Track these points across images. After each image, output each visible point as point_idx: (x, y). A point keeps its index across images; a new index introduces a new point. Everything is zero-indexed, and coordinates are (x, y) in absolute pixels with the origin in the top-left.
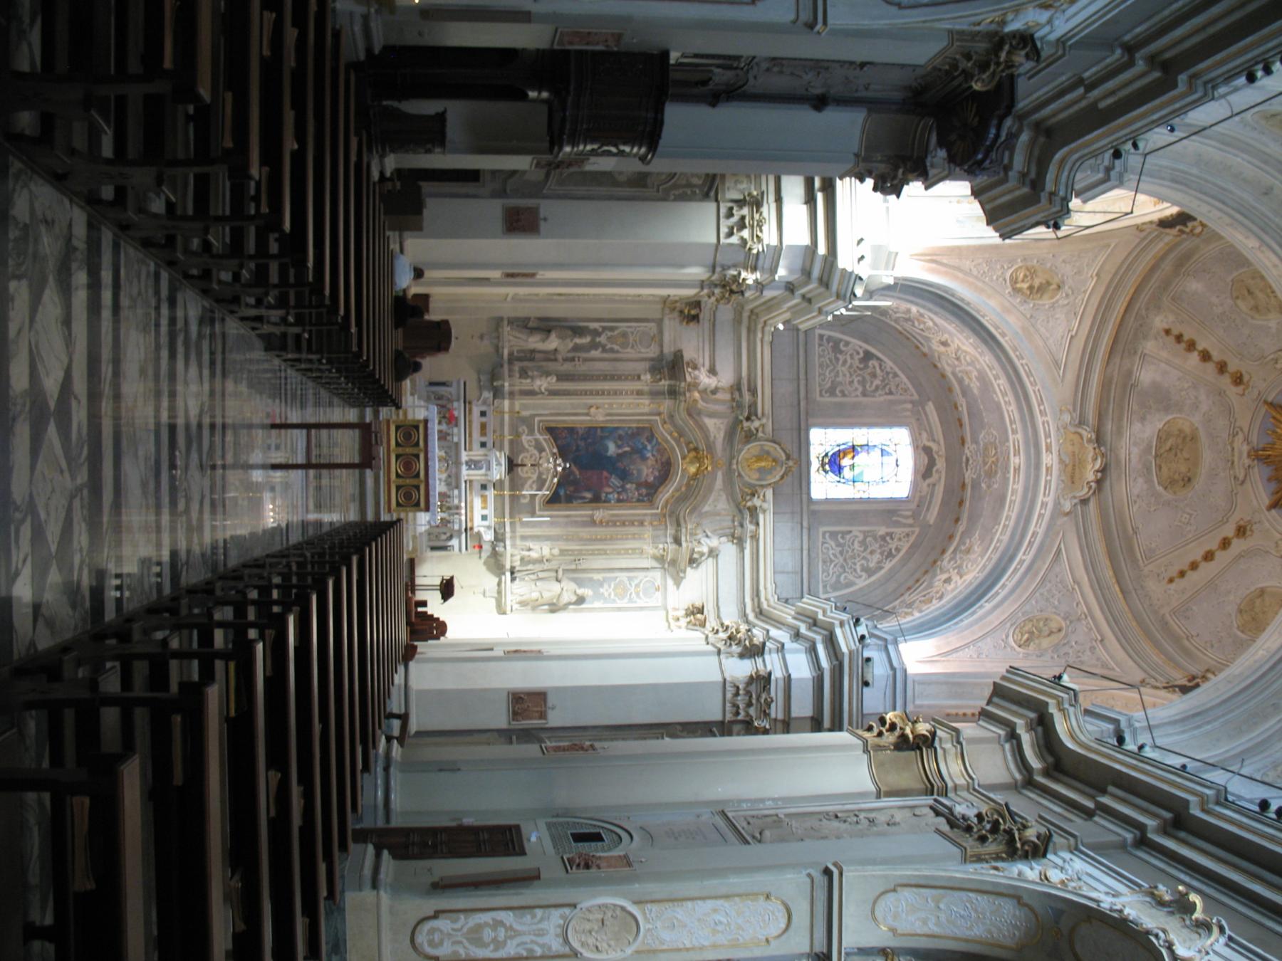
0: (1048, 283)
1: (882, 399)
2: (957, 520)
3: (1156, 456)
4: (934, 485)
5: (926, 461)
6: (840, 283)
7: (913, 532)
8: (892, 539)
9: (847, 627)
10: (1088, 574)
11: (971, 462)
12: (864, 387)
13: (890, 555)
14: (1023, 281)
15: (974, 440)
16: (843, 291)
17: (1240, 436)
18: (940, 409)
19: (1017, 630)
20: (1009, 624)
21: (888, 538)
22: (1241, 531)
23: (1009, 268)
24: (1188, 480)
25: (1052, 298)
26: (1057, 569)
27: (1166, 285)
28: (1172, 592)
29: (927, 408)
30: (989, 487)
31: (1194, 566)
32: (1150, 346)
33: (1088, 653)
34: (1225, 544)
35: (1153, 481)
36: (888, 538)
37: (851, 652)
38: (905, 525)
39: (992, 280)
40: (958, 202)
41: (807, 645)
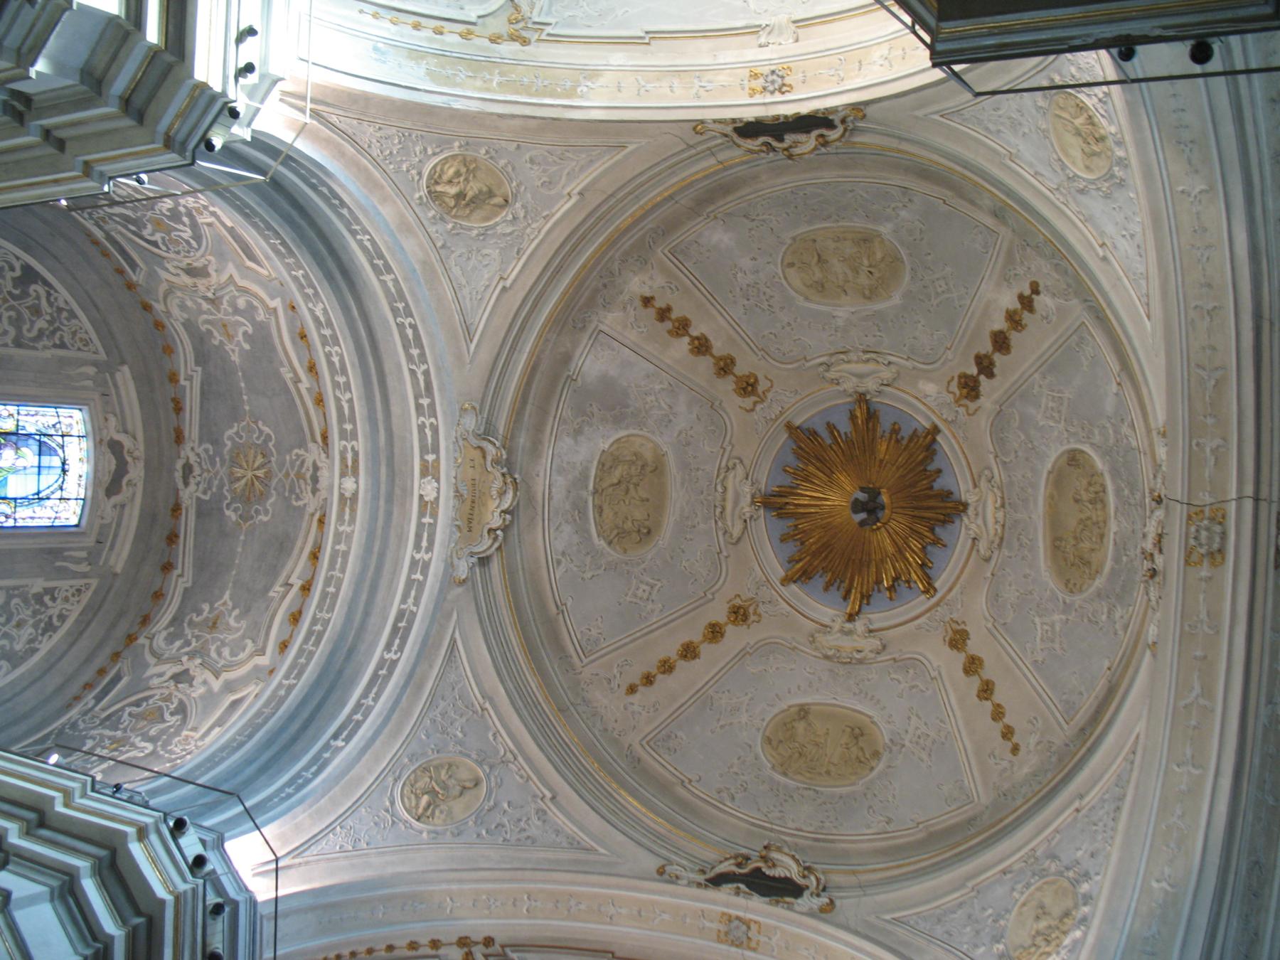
0: (491, 194)
1: (48, 354)
2: (167, 567)
3: (595, 492)
4: (123, 506)
5: (113, 467)
6: (183, 115)
7: (88, 586)
8: (54, 599)
9: (154, 838)
10: (502, 682)
11: (197, 471)
12: (19, 329)
13: (50, 628)
14: (450, 182)
15: (210, 434)
16: (180, 137)
17: (740, 470)
18: (144, 381)
19: (407, 789)
20: (390, 779)
21: (47, 599)
22: (739, 614)
23: (434, 154)
24: (647, 533)
25: (487, 219)
26: (452, 677)
27: (670, 226)
28: (636, 708)
29: (118, 376)
30: (245, 517)
31: (667, 667)
32: (611, 320)
33: (535, 820)
34: (715, 632)
35: (588, 531)
36: (47, 599)
37: (178, 898)
38: (75, 575)
39: (398, 171)
40: (375, 16)
41: (55, 883)
